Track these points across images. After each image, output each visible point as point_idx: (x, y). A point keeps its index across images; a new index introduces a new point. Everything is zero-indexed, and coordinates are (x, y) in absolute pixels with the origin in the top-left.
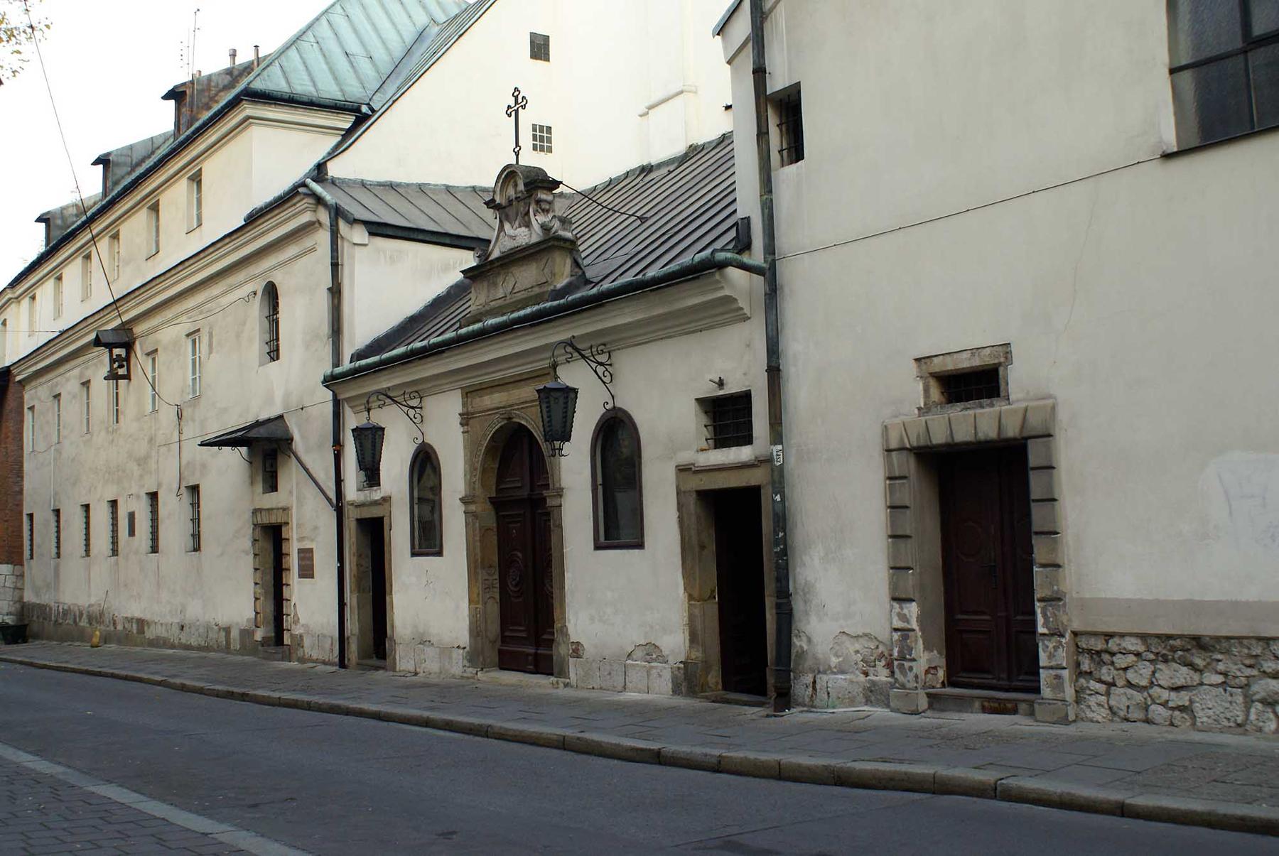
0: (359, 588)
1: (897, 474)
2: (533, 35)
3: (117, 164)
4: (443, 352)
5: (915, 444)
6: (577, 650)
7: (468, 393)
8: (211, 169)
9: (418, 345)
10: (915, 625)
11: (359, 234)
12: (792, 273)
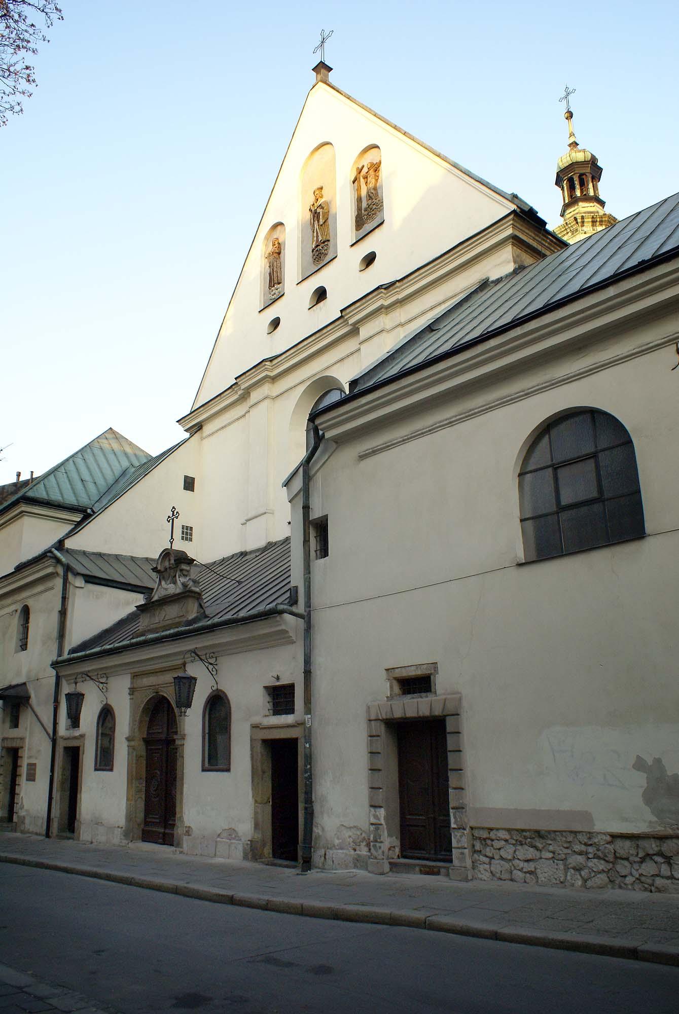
5: (384, 717)
6: (188, 832)
7: (135, 676)
10: (383, 822)
11: (79, 582)
12: (321, 619)
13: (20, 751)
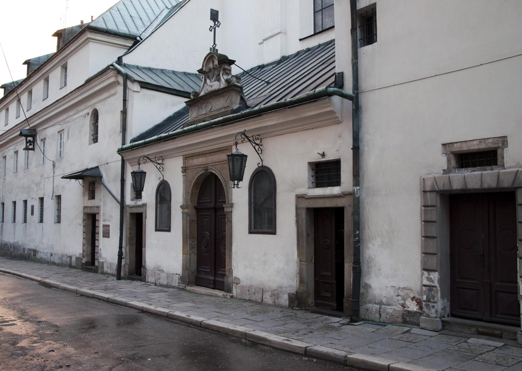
0: (130, 243)
1: (430, 204)
2: (212, 10)
3: (33, 64)
4: (176, 138)
5: (441, 188)
6: (237, 281)
7: (186, 158)
8: (71, 63)
9: (163, 135)
10: (436, 284)
11: (136, 87)
12: (368, 101)
13: (97, 216)
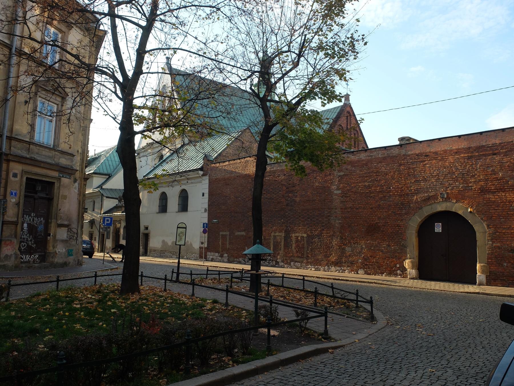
11: (105, 198)
